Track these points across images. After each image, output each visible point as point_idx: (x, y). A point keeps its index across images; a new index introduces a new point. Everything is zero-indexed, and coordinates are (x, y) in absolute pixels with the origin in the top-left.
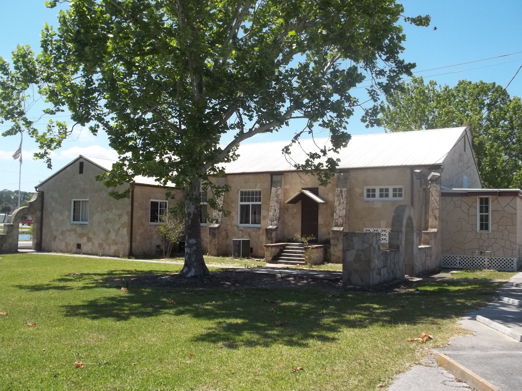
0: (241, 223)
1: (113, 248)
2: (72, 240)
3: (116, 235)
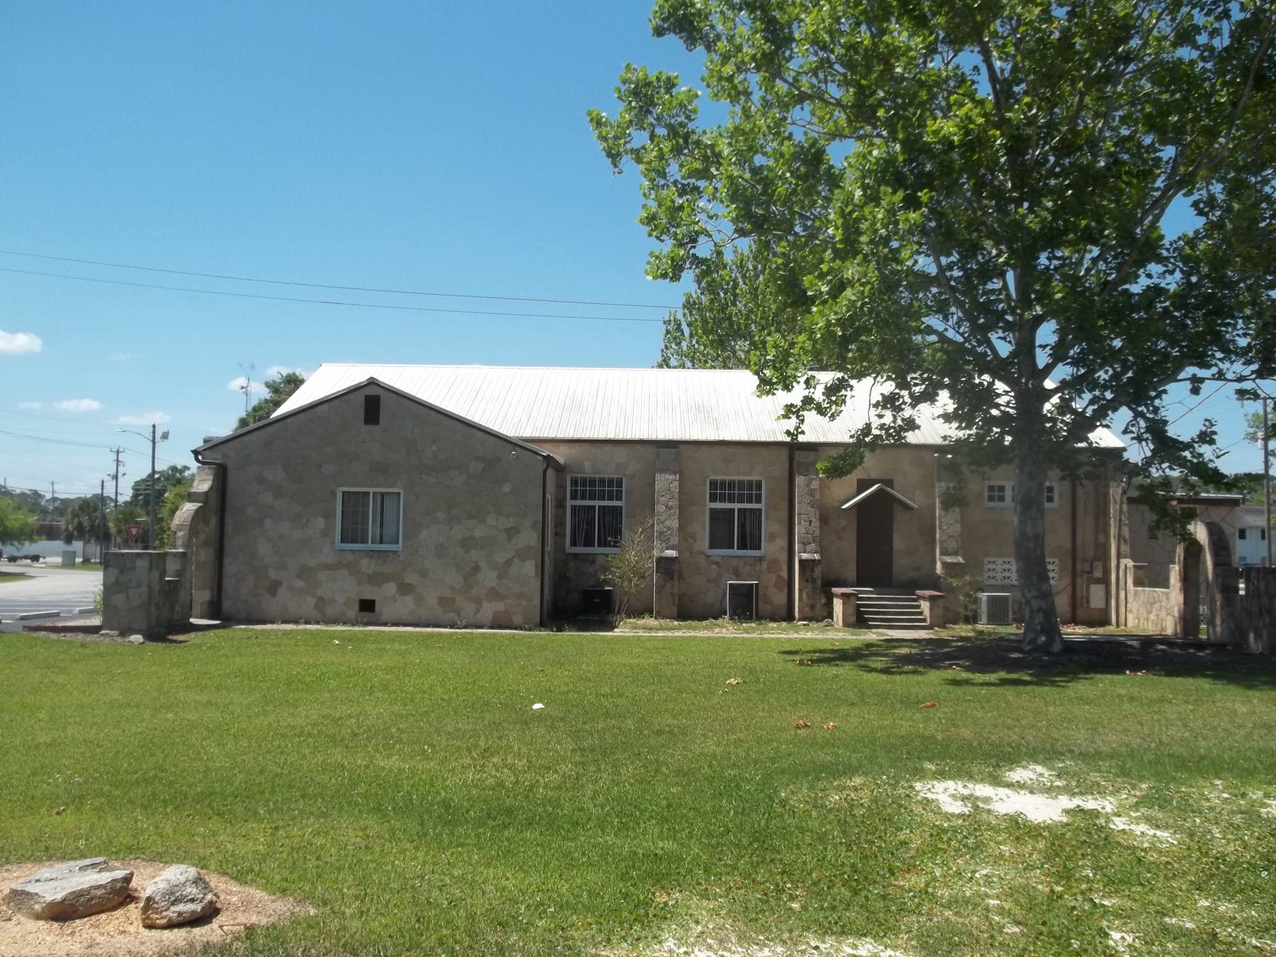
0: (711, 547)
1: (489, 610)
2: (346, 590)
3: (500, 577)
